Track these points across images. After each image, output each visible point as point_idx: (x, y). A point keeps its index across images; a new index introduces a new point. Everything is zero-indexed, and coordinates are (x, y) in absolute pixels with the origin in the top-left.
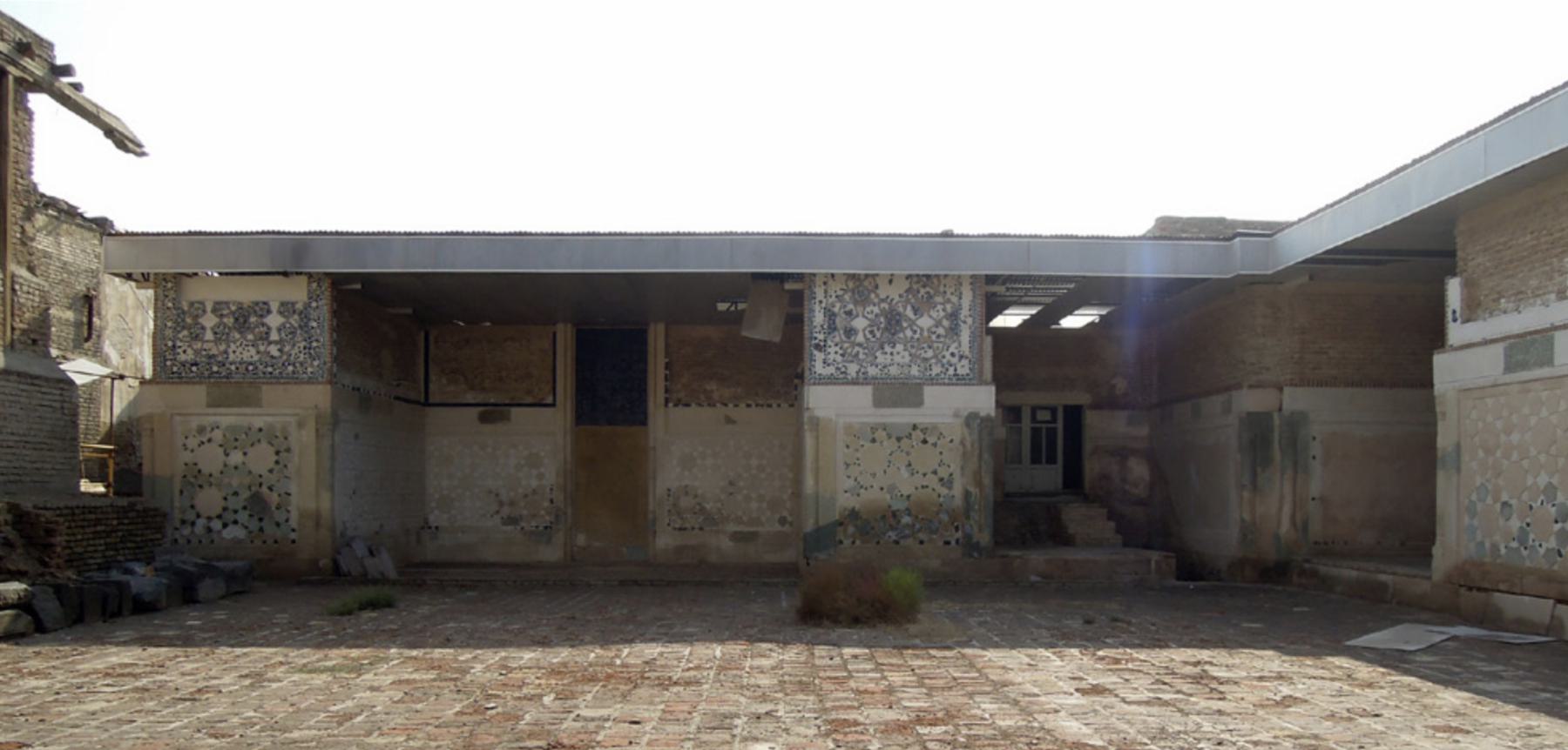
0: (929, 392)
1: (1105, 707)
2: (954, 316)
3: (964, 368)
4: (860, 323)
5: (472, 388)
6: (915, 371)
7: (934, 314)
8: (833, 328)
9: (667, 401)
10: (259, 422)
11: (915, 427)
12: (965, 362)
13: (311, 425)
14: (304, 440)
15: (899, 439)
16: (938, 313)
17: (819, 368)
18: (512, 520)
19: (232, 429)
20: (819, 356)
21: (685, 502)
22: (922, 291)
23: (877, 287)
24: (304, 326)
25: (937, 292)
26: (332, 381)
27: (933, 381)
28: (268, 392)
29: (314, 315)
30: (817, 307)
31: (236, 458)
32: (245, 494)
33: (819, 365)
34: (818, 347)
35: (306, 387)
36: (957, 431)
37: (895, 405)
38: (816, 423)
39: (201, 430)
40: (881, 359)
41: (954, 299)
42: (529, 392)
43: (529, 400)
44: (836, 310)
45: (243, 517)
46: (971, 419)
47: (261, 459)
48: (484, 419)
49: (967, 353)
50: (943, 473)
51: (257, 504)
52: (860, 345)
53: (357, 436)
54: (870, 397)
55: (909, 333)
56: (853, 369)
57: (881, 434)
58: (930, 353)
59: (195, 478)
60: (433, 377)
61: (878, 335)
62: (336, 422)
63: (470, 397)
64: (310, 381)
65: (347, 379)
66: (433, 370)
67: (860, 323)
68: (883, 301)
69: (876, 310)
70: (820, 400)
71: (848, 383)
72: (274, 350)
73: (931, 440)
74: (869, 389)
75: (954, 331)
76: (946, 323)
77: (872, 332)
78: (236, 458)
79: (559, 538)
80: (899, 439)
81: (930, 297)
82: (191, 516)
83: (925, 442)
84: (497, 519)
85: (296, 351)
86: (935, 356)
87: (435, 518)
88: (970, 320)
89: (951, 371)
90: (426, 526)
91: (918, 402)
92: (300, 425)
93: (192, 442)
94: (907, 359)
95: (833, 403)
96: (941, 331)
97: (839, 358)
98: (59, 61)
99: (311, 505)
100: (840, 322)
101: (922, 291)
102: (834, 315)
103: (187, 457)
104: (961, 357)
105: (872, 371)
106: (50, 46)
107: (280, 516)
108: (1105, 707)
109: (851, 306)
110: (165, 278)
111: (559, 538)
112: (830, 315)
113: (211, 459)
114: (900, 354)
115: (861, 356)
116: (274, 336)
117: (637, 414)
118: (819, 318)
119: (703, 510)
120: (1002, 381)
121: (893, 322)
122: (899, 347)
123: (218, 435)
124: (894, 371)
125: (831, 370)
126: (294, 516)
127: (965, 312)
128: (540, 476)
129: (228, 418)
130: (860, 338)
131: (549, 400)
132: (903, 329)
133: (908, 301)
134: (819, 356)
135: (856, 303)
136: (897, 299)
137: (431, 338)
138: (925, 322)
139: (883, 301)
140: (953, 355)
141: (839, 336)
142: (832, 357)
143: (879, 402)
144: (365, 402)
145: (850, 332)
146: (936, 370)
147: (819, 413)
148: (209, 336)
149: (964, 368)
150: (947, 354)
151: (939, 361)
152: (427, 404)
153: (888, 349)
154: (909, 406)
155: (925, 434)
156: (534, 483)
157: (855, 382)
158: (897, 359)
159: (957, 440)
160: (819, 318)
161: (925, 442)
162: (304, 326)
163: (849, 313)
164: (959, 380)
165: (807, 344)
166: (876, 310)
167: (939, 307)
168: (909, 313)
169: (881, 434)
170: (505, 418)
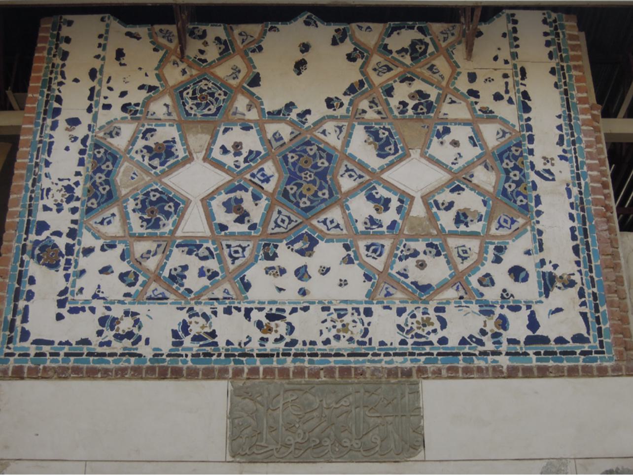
1: (108, 344)
2: (511, 157)
3: (562, 317)
4: (194, 180)
6: (385, 327)
7: (442, 151)
8: (102, 195)
12: (560, 297)
16: (458, 148)
17: (42, 320)
20: (47, 282)
22: (402, 92)
23: (255, 81)
25: (448, 93)
27: (461, 362)
30: (61, 136)
34: (49, 256)
40: (262, 287)
41: (508, 112)
44: (120, 143)
49: (567, 265)
52: (191, 246)
54: (219, 426)
55: (361, 208)
56: (159, 324)
58: (437, 271)
61: (256, 213)
67: (194, 180)
68: (275, 115)
69: (251, 141)
71: (137, 373)
74: (217, 392)
75: (516, 197)
76: (485, 178)
77: (234, 206)
86: (458, 280)
88: (563, 171)
89: (518, 327)
94: (358, 289)
96: (468, 200)
97: (114, 288)
100: (128, 179)
101: (402, 92)
102: (113, 157)
104: (548, 283)
105: (231, 329)
108: (108, 344)
109: (166, 133)
112: (101, 159)
114: (334, 275)
115: (193, 281)
120: (24, 107)
122: (328, 253)
124: (309, 327)
125: (83, 326)
127: (545, 146)
130: (194, 224)
132: (337, 198)
133: (357, 115)
134: (47, 282)
135: (184, 124)
136: (319, 110)
138: (414, 175)
139: (275, 115)
140: (517, 273)
142: (89, 283)
145: (159, 206)
146: (463, 323)
149: (562, 317)
150: (501, 273)
151: (467, 296)
153: (287, 258)
157: (162, 370)
158: (321, 288)
159: (68, 81)
160: (64, 164)
163: (164, 152)
164: (544, 357)
166: (251, 141)
167: (461, 133)
168: (361, 147)
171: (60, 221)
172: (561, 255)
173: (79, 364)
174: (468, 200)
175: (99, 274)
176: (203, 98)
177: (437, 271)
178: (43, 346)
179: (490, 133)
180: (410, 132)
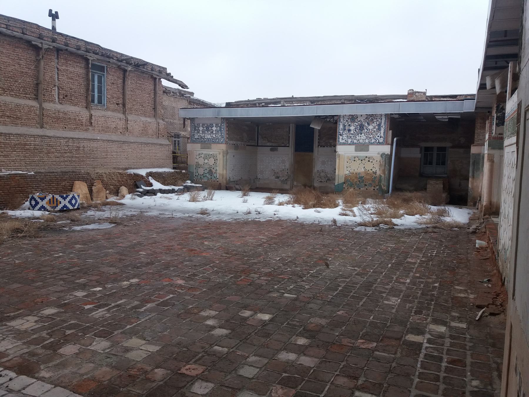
0: (371, 147)
2: (379, 125)
3: (381, 140)
4: (352, 128)
5: (269, 141)
6: (367, 141)
9: (318, 146)
10: (211, 153)
11: (366, 157)
12: (382, 138)
13: (222, 154)
14: (220, 157)
15: (362, 160)
16: (375, 124)
17: (341, 141)
18: (278, 177)
19: (205, 154)
20: (341, 137)
21: (322, 174)
24: (220, 130)
26: (226, 143)
27: (372, 144)
28: (213, 146)
29: (223, 127)
31: (206, 161)
32: (208, 170)
33: (341, 140)
34: (341, 135)
35: (221, 145)
36: (379, 158)
37: (361, 151)
38: (339, 156)
39: (199, 154)
40: (358, 138)
41: (380, 120)
42: (283, 143)
43: (283, 145)
45: (207, 175)
46: (382, 155)
47: (211, 161)
48: (272, 150)
50: (374, 170)
51: (210, 172)
53: (234, 156)
55: (366, 130)
56: (350, 141)
57: (357, 159)
58: (372, 136)
59: (198, 166)
60: (259, 139)
62: (227, 153)
63: (268, 144)
64: (221, 143)
65: (232, 142)
66: (260, 137)
67: (352, 128)
69: (357, 124)
70: (340, 149)
72: (214, 136)
73: (371, 161)
74: (354, 146)
75: (379, 129)
78: (206, 161)
79: (289, 183)
80: (362, 160)
81: (372, 119)
82: (197, 174)
83: (369, 161)
84: (274, 177)
85: (219, 136)
86: (373, 137)
87: (259, 176)
88: (384, 126)
89: (378, 141)
90: (257, 178)
91: (368, 150)
92: (219, 154)
93: (198, 157)
95: (345, 151)
96: (375, 130)
97: (346, 138)
98: (168, 72)
99: (221, 173)
100: (347, 128)
101: (370, 118)
103: (196, 160)
105: (355, 141)
106: (165, 69)
107: (215, 175)
109: (350, 123)
110: (192, 118)
111: (289, 183)
112: (344, 126)
113: (201, 161)
114: (363, 136)
116: (214, 132)
117: (311, 150)
118: (341, 127)
119: (327, 176)
121: (362, 127)
122: (363, 135)
123: (203, 156)
124: (361, 141)
125: (344, 141)
126: (218, 175)
127: (383, 124)
128: (285, 166)
129: (205, 152)
130: (352, 132)
131: (288, 145)
132: (364, 129)
134: (341, 137)
135: (351, 122)
137: (259, 128)
138: (371, 127)
141: (346, 132)
143: (356, 150)
144: (236, 147)
145: (349, 130)
146: (373, 141)
147: (340, 153)
148: (201, 132)
149: (381, 140)
152: (258, 146)
153: (360, 135)
154: (365, 151)
155: (369, 159)
156: (283, 167)
157: (350, 145)
158: (362, 138)
159: (378, 161)
160: (341, 127)
161: (369, 161)
162: (220, 130)
163: (349, 125)
164: (379, 143)
165: (338, 134)
166: (357, 124)
168: (366, 125)
169: (357, 159)
170: (277, 150)
171: (341, 132)
172: (382, 135)
173: (344, 144)
174: (375, 130)
175: (345, 137)
176: (353, 120)
177: (372, 136)
178: (315, 170)
179: (378, 123)
180: (370, 123)
